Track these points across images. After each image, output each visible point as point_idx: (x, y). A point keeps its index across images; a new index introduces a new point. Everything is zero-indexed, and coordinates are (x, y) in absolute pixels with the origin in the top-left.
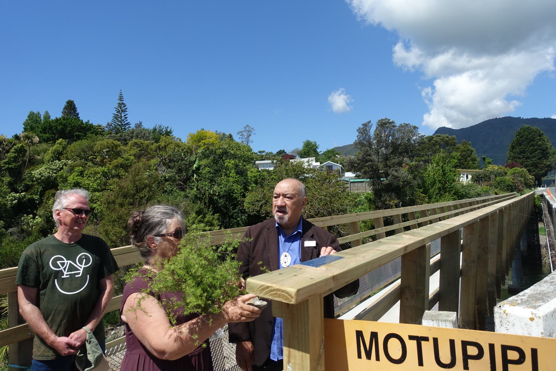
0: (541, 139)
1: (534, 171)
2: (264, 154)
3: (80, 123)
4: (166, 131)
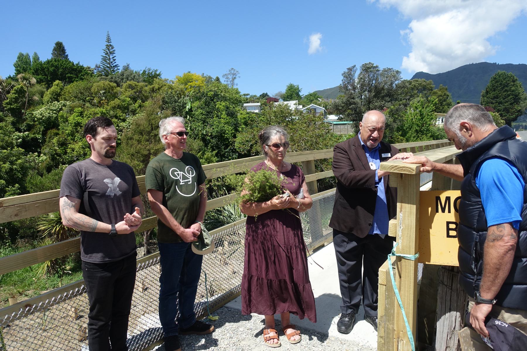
1: (505, 116)
2: (248, 97)
3: (71, 64)
4: (155, 74)
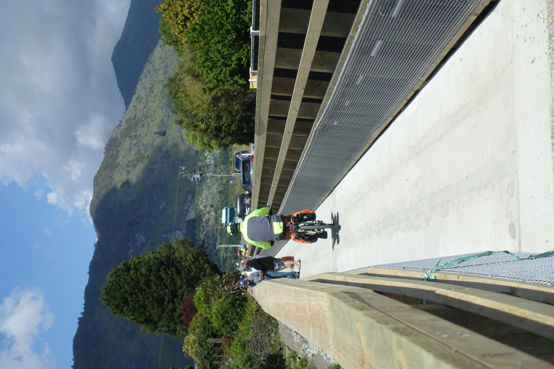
0: (135, 269)
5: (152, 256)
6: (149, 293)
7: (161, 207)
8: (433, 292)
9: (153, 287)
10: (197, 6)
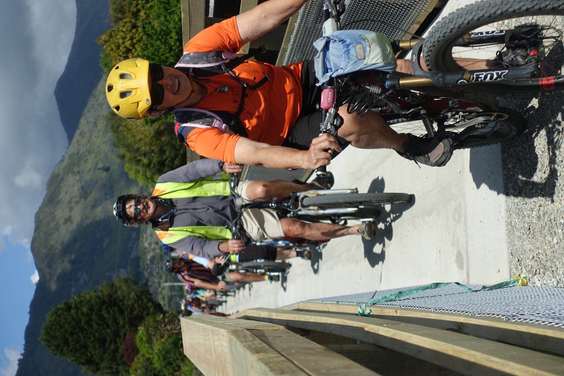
0: (77, 308)
5: (93, 294)
6: (91, 333)
7: (104, 245)
8: (362, 329)
9: (95, 326)
10: (139, 37)
